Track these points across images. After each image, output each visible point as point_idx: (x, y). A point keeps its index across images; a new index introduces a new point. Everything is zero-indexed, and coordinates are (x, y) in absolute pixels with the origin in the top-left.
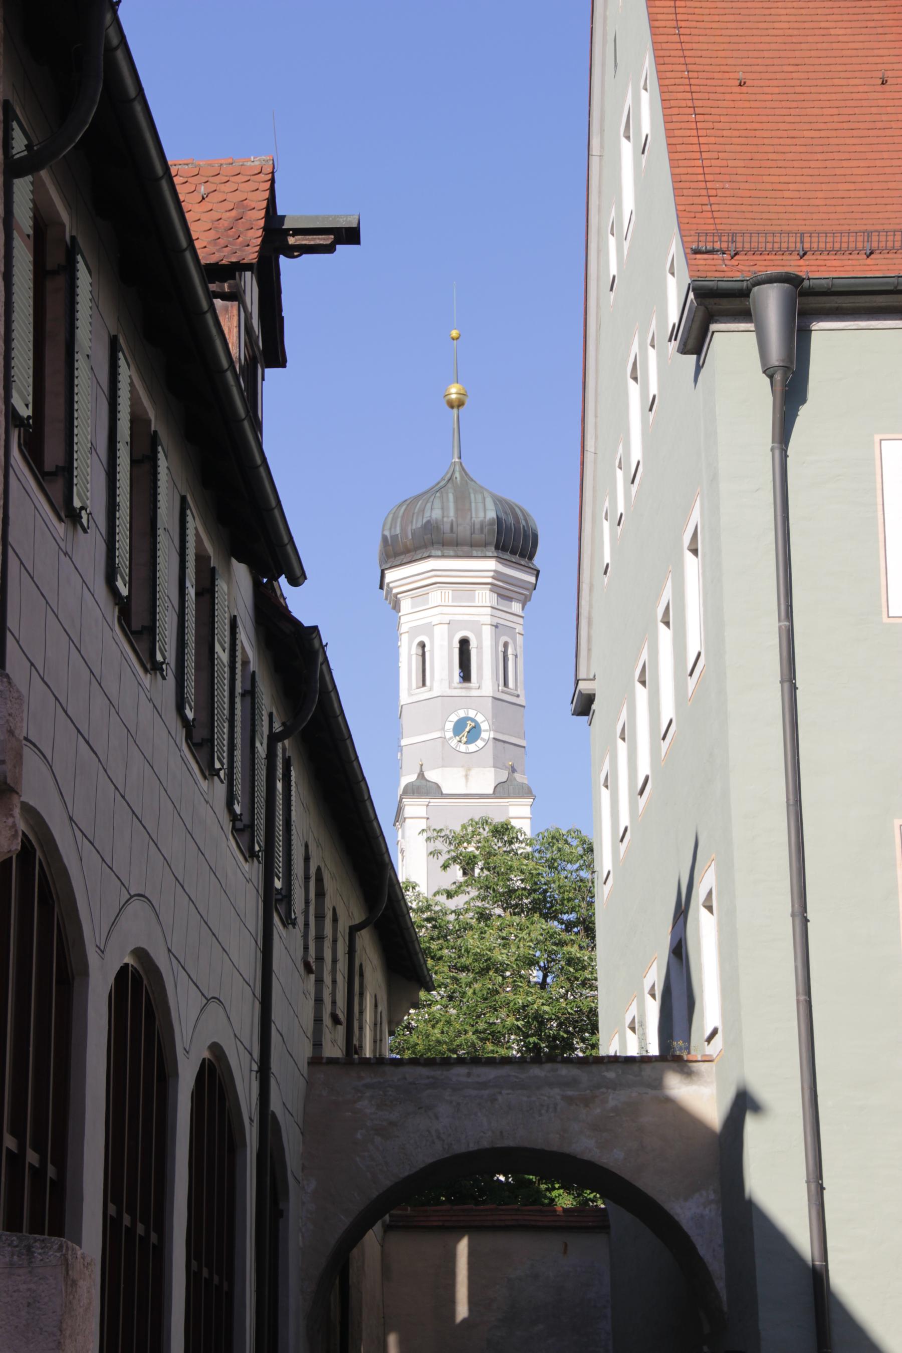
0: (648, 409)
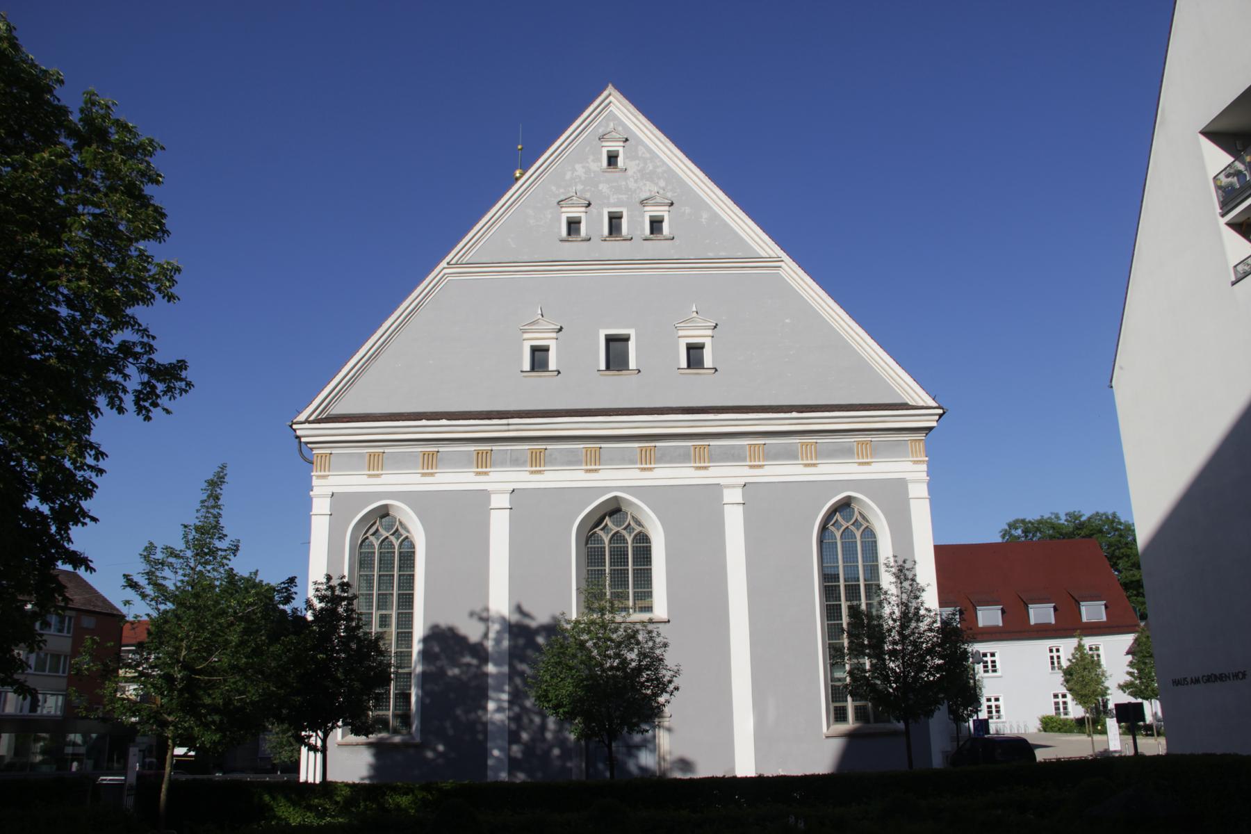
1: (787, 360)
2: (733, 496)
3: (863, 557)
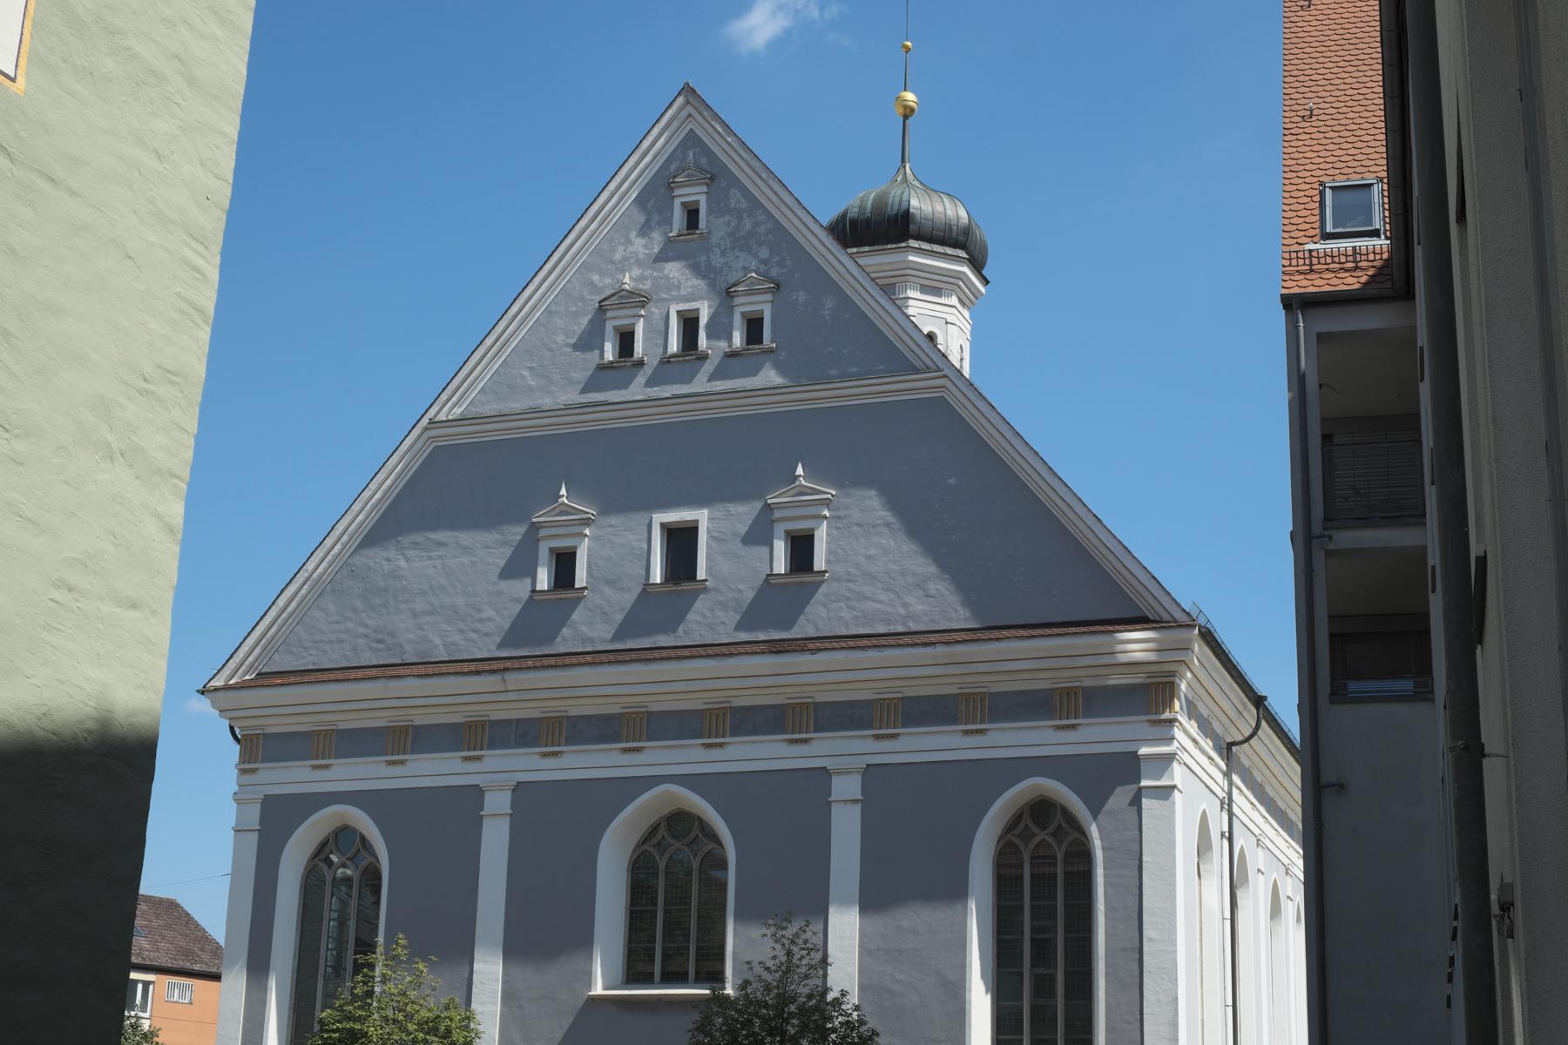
2: (846, 787)
3: (1032, 893)
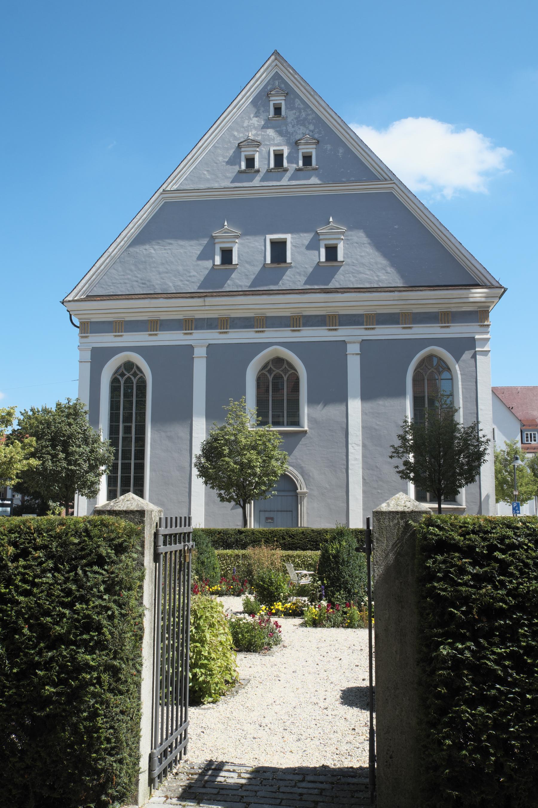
0: (495, 502)
1: (394, 255)
2: (353, 349)
